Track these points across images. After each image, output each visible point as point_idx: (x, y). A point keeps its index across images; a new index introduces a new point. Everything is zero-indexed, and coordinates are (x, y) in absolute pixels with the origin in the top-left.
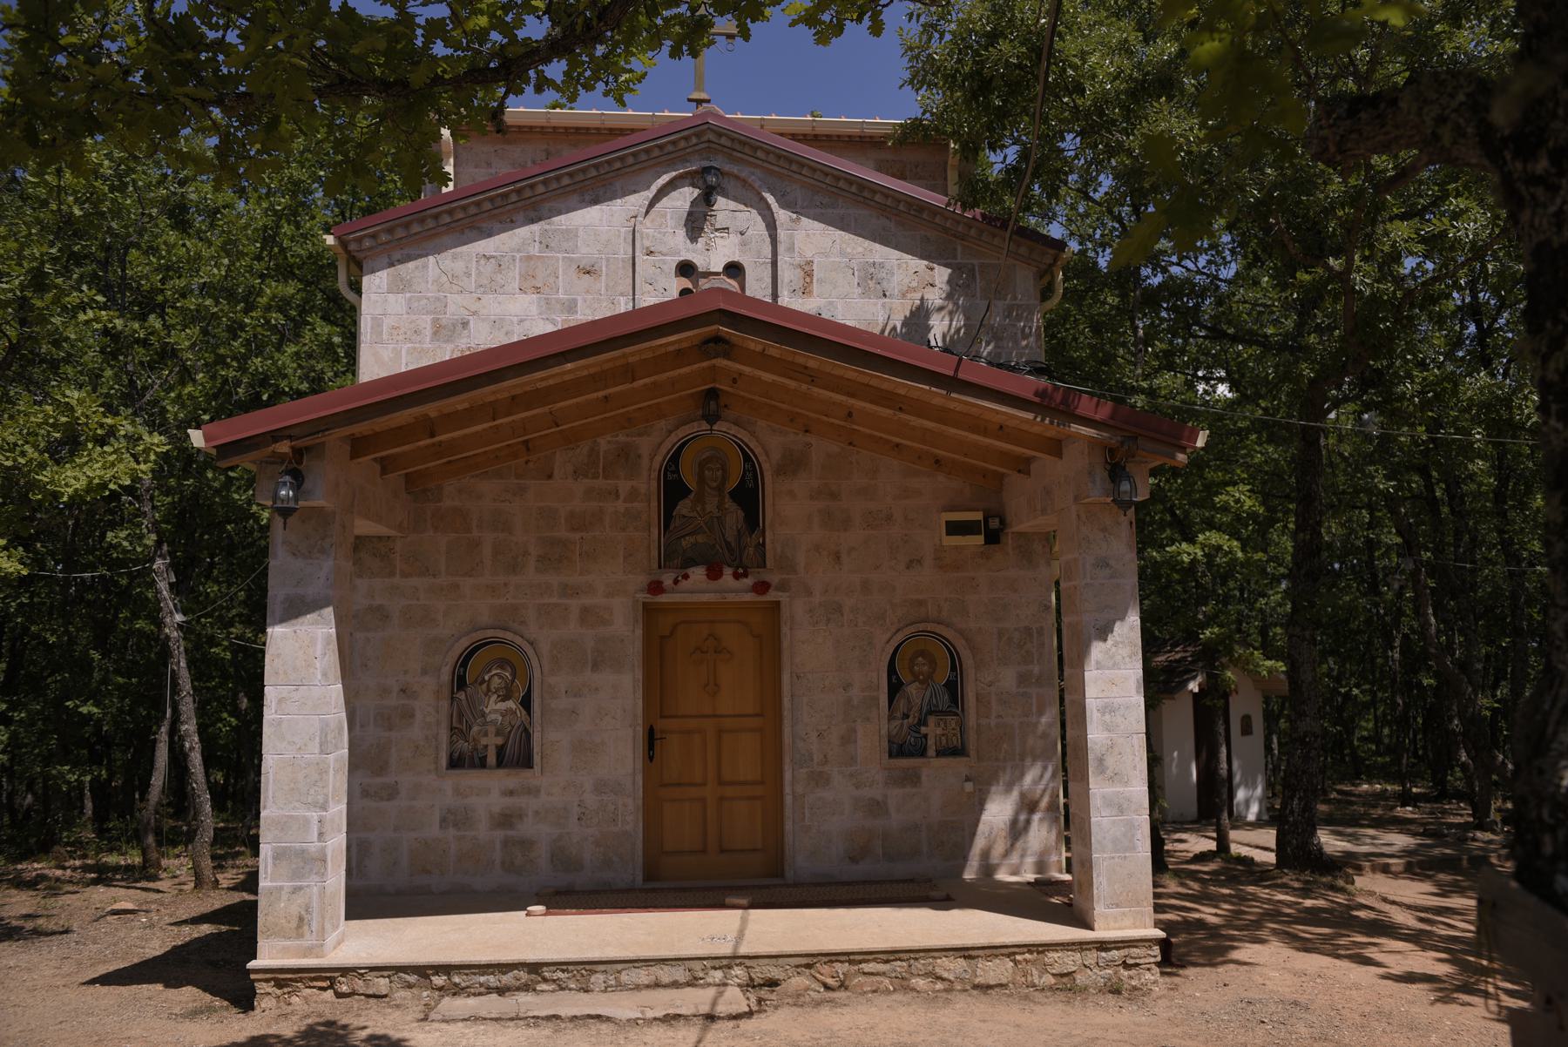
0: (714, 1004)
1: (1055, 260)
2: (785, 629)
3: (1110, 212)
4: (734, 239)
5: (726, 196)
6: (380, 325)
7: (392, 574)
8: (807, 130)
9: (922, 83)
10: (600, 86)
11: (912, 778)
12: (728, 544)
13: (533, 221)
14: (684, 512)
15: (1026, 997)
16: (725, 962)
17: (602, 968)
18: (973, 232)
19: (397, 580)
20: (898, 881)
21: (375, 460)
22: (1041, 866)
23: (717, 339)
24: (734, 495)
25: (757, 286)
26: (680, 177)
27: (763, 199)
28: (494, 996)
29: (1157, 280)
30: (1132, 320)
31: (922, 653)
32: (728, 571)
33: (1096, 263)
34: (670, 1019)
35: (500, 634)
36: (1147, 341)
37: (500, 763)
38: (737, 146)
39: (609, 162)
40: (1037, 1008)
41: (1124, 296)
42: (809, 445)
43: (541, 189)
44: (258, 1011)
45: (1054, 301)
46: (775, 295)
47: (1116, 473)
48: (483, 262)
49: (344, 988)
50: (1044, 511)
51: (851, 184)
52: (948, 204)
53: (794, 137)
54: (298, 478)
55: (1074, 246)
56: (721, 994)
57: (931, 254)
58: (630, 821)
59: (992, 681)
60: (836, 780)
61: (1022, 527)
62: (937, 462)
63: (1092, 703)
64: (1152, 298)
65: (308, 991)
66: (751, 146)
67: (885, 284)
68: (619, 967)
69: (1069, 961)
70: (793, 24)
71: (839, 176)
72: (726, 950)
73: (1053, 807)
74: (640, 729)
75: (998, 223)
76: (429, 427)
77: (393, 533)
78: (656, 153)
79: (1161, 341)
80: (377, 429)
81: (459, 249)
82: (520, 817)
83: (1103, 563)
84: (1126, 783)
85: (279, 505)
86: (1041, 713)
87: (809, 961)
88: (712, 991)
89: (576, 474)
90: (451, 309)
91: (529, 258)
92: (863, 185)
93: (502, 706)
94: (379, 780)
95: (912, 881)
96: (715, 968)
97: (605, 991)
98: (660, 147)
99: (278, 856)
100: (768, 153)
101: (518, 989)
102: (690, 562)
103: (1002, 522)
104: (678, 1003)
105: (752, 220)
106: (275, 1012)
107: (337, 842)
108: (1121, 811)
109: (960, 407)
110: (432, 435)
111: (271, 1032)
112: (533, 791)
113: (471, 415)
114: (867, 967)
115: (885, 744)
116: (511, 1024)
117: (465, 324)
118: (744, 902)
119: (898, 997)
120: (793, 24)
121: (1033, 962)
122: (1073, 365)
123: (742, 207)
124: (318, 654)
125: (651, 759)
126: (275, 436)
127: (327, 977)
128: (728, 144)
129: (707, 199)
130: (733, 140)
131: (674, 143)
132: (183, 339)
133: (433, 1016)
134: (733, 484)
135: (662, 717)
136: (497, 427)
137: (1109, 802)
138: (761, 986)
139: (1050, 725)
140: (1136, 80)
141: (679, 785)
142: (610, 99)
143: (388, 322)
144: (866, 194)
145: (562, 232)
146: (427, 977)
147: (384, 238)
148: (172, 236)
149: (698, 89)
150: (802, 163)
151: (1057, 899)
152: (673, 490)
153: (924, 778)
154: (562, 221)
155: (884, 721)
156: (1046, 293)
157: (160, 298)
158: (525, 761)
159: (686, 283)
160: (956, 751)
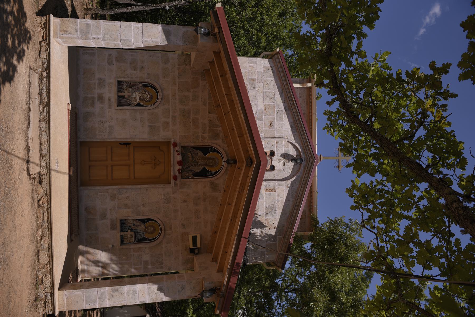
0: (33, 163)
1: (279, 267)
2: (162, 185)
3: (293, 282)
4: (282, 168)
5: (294, 165)
6: (254, 63)
7: (179, 65)
8: (314, 190)
9: (329, 223)
10: (329, 122)
11: (113, 227)
12: (189, 167)
13: (285, 108)
14: (199, 154)
15: (34, 268)
16: (48, 167)
17: (47, 126)
18: (286, 240)
19: (177, 66)
20: (78, 224)
21: (213, 60)
22: (83, 271)
23: (252, 162)
24: (204, 169)
25: (268, 175)
26: (299, 152)
27: (294, 176)
28: (39, 91)
29: (273, 297)
30: (261, 291)
31: (154, 230)
32: (180, 167)
33: (278, 278)
34: (28, 148)
35: (160, 97)
36: (255, 295)
37: (119, 97)
38: (309, 168)
39: (303, 131)
40: (29, 272)
41: (268, 288)
42: (220, 192)
43: (294, 111)
44: (36, 17)
45: (266, 267)
46: (265, 180)
47: (213, 291)
48: (273, 93)
49: (43, 44)
50: (200, 267)
51: (299, 203)
52: (294, 232)
53: (312, 186)
54: (207, 34)
55: (283, 271)
56: (37, 165)
57: (280, 229)
58: (100, 137)
59: (145, 252)
60: (109, 203)
61: (195, 261)
62: (216, 232)
63: (136, 287)
64: (267, 296)
65: (42, 33)
66: (309, 172)
67: (269, 214)
68: (48, 132)
69: (47, 283)
70: (352, 181)
71: (301, 199)
72: (53, 167)
73: (103, 274)
74: (130, 140)
75: (289, 250)
76: (223, 75)
77: (191, 65)
78: (306, 144)
79: (255, 300)
80: (223, 59)
81: (276, 87)
82: (101, 103)
83: (183, 288)
84: (109, 300)
85: (199, 29)
86: (135, 269)
87: (48, 195)
88: (38, 162)
89: (210, 121)
90: (259, 84)
91: (274, 107)
92: (299, 206)
93: (138, 97)
94: (114, 59)
95: (79, 228)
96: (46, 163)
97: (39, 127)
98: (308, 146)
99: (87, 25)
100: (307, 177)
101: (41, 99)
102: (183, 156)
103: (197, 254)
104: (34, 151)
105: (288, 173)
106: (35, 22)
107: (92, 44)
108: (100, 298)
109: (232, 239)
110: (221, 76)
111: (28, 19)
112: (110, 106)
113: (227, 87)
114: (46, 214)
115: (124, 218)
116: (28, 96)
117: (254, 88)
118: (71, 173)
119: (35, 225)
120: (352, 181)
121: (47, 270)
122: (247, 273)
123: (291, 170)
124: (152, 39)
125: (120, 144)
126: (220, 28)
127: (47, 39)
128: (309, 166)
129: (293, 160)
130: (311, 167)
131: (309, 150)
132: (249, 12)
133: (31, 71)
134: (208, 168)
135: (134, 147)
136: (224, 96)
137: (103, 294)
138: (40, 179)
139: (131, 272)
140: (334, 289)
141: (112, 152)
142: (325, 125)
143: (255, 66)
144: (296, 207)
145: (282, 117)
146: (46, 70)
147: (279, 65)
148: (277, 11)
149: (323, 158)
150: (304, 188)
151: (71, 277)
152: (205, 150)
153: (114, 231)
154: (285, 117)
155: (132, 218)
156: (269, 264)
157: (260, 7)
158: (120, 104)
159: (268, 154)
160: (122, 242)
